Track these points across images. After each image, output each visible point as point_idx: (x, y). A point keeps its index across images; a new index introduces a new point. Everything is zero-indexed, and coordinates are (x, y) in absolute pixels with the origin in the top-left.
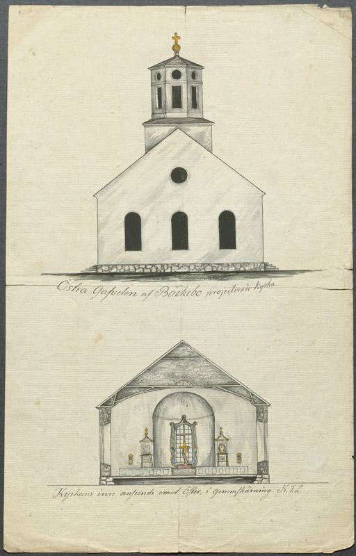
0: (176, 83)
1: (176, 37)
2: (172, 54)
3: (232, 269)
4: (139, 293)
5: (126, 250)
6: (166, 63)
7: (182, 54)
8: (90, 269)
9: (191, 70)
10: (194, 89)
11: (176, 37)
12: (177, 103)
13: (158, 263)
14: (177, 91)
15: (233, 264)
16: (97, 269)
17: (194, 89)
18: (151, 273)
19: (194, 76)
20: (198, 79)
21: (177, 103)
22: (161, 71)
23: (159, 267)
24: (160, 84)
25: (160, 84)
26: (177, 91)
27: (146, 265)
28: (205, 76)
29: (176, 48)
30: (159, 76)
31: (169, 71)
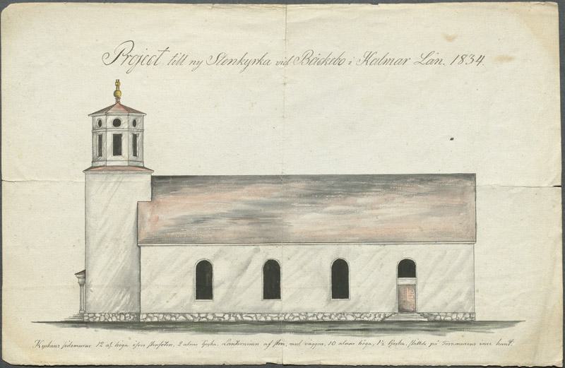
0: (117, 131)
1: (118, 82)
2: (113, 101)
3: (181, 318)
4: (338, 342)
5: (198, 298)
6: (105, 111)
7: (123, 102)
8: (75, 317)
9: (132, 119)
10: (135, 137)
11: (118, 82)
12: (117, 150)
13: (203, 311)
14: (117, 139)
15: (184, 314)
16: (83, 317)
17: (135, 137)
18: (252, 321)
19: (134, 123)
20: (138, 126)
21: (117, 150)
22: (103, 118)
23: (238, 316)
24: (101, 132)
25: (101, 132)
26: (117, 139)
27: (446, 313)
28: (148, 123)
29: (118, 98)
30: (100, 123)
31: (111, 119)
